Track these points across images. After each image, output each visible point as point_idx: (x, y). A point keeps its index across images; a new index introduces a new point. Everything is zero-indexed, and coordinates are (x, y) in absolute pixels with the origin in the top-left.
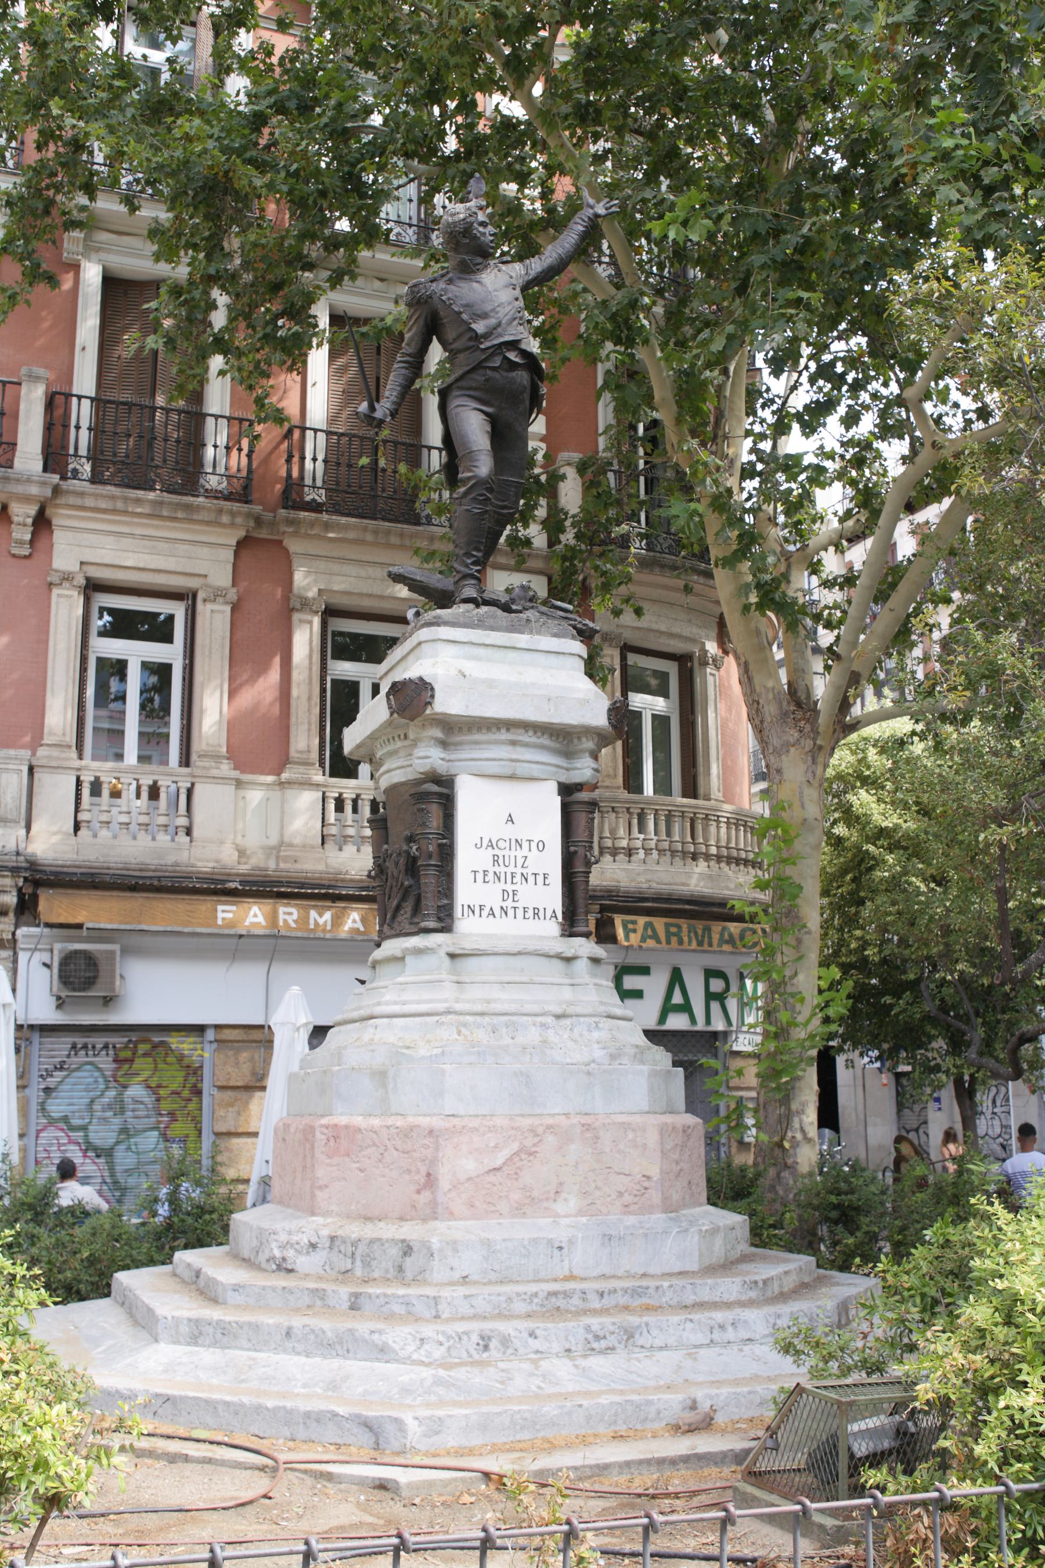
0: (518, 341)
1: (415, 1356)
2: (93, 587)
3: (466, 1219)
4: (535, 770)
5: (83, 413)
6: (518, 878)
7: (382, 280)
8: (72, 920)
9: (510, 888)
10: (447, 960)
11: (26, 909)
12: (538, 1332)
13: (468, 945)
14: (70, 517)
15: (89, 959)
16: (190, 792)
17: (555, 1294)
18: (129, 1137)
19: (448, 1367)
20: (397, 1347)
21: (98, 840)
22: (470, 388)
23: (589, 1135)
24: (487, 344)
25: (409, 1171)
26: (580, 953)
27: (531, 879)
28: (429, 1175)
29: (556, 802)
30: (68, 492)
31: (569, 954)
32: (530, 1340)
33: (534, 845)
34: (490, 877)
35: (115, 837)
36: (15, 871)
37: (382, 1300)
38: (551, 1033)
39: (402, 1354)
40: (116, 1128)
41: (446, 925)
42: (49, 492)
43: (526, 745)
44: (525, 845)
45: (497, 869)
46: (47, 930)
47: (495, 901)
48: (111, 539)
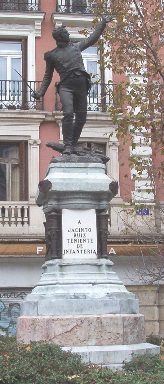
0: (79, 68)
9: (80, 244)
13: (66, 262)
16: (28, 210)
18: (13, 324)
22: (64, 85)
24: (69, 70)
27: (87, 241)
34: (73, 240)
40: (9, 321)
41: (60, 257)
43: (80, 198)
44: (85, 230)
45: (75, 238)
47: (75, 249)
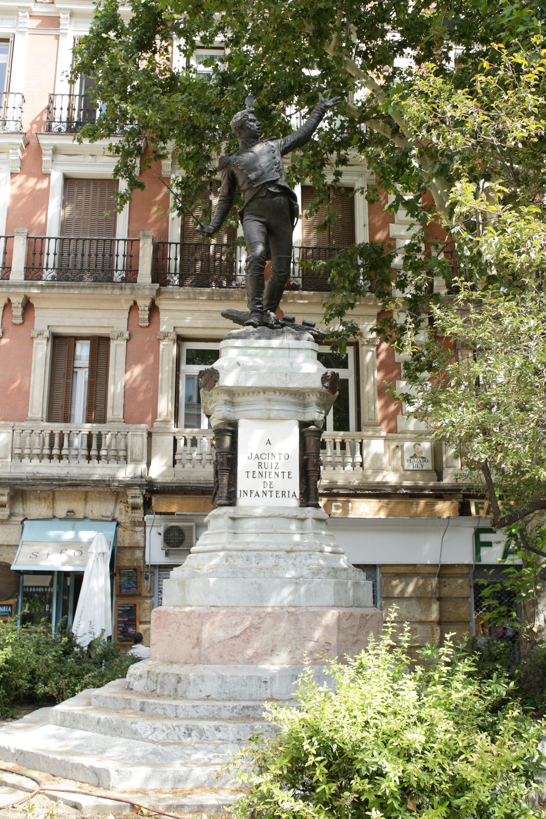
1: (150, 738)
2: (181, 339)
3: (217, 664)
4: (282, 414)
5: (173, 252)
6: (273, 475)
7: (92, 156)
8: (169, 511)
10: (230, 521)
11: (147, 506)
12: (221, 728)
13: (241, 513)
14: (167, 304)
15: (180, 531)
17: (247, 707)
19: (164, 744)
20: (141, 732)
21: (185, 469)
23: (292, 618)
25: (189, 637)
26: (308, 516)
27: (281, 475)
28: (198, 639)
29: (296, 430)
30: (165, 292)
31: (302, 516)
32: (216, 732)
33: (282, 456)
34: (257, 474)
35: (193, 467)
36: (140, 486)
37: (154, 706)
38: (281, 560)
39: (144, 736)
42: (154, 293)
44: (277, 456)
45: (260, 470)
46: (157, 516)
48: (189, 313)
